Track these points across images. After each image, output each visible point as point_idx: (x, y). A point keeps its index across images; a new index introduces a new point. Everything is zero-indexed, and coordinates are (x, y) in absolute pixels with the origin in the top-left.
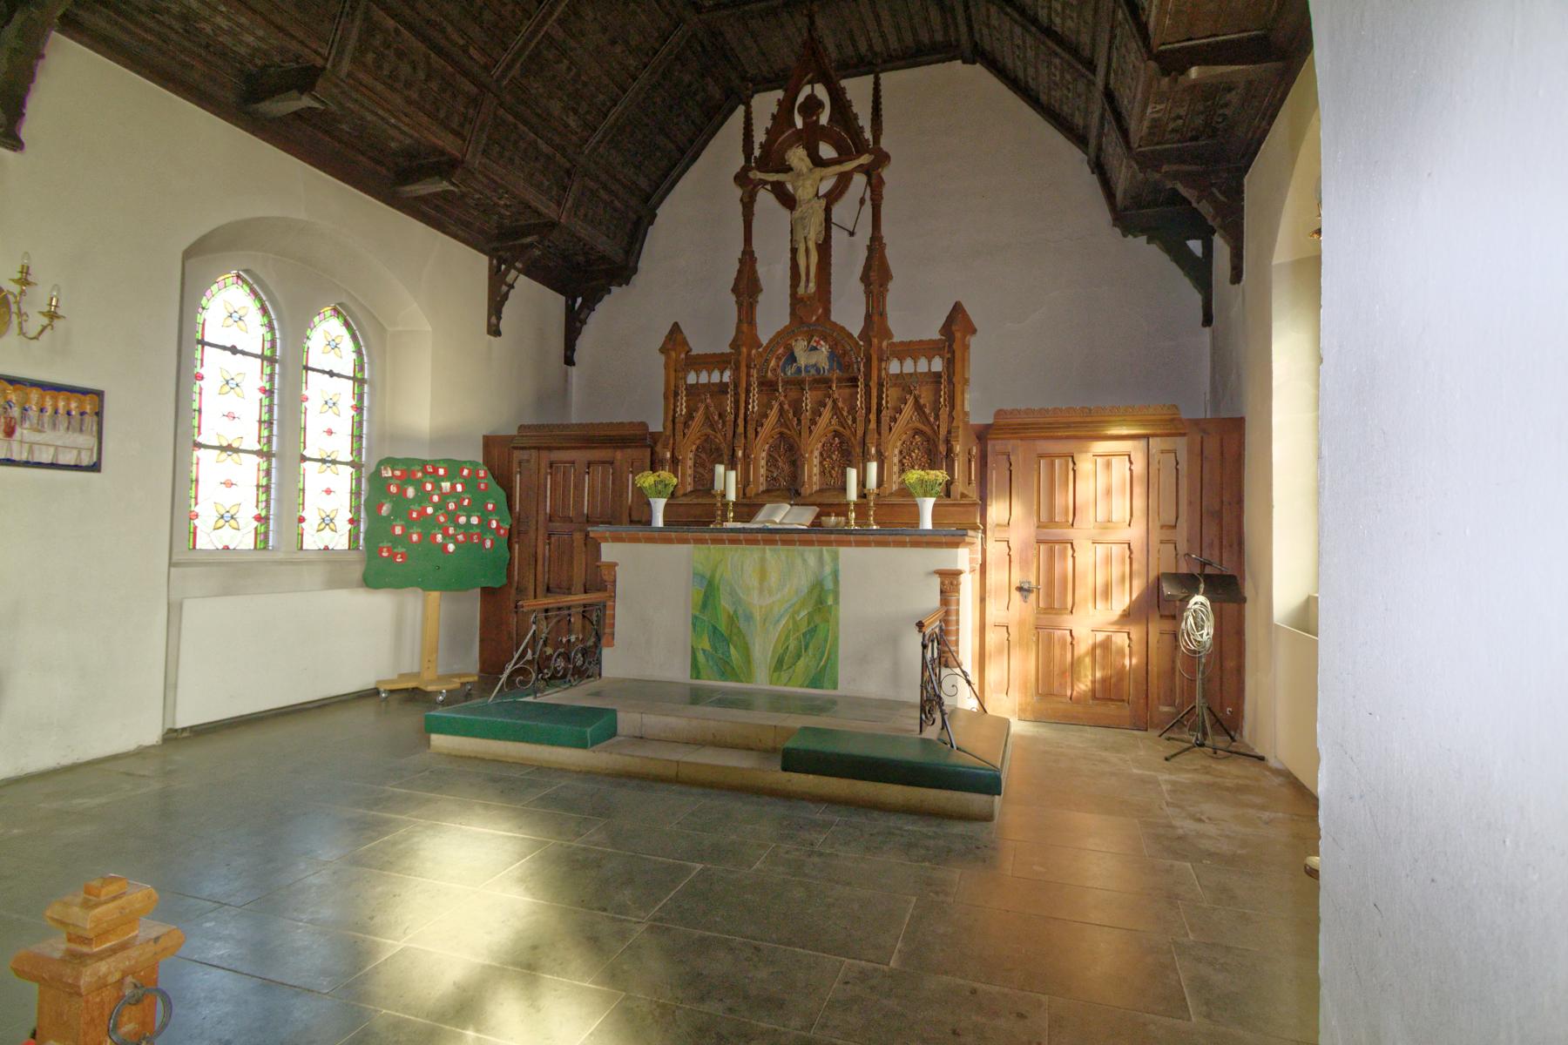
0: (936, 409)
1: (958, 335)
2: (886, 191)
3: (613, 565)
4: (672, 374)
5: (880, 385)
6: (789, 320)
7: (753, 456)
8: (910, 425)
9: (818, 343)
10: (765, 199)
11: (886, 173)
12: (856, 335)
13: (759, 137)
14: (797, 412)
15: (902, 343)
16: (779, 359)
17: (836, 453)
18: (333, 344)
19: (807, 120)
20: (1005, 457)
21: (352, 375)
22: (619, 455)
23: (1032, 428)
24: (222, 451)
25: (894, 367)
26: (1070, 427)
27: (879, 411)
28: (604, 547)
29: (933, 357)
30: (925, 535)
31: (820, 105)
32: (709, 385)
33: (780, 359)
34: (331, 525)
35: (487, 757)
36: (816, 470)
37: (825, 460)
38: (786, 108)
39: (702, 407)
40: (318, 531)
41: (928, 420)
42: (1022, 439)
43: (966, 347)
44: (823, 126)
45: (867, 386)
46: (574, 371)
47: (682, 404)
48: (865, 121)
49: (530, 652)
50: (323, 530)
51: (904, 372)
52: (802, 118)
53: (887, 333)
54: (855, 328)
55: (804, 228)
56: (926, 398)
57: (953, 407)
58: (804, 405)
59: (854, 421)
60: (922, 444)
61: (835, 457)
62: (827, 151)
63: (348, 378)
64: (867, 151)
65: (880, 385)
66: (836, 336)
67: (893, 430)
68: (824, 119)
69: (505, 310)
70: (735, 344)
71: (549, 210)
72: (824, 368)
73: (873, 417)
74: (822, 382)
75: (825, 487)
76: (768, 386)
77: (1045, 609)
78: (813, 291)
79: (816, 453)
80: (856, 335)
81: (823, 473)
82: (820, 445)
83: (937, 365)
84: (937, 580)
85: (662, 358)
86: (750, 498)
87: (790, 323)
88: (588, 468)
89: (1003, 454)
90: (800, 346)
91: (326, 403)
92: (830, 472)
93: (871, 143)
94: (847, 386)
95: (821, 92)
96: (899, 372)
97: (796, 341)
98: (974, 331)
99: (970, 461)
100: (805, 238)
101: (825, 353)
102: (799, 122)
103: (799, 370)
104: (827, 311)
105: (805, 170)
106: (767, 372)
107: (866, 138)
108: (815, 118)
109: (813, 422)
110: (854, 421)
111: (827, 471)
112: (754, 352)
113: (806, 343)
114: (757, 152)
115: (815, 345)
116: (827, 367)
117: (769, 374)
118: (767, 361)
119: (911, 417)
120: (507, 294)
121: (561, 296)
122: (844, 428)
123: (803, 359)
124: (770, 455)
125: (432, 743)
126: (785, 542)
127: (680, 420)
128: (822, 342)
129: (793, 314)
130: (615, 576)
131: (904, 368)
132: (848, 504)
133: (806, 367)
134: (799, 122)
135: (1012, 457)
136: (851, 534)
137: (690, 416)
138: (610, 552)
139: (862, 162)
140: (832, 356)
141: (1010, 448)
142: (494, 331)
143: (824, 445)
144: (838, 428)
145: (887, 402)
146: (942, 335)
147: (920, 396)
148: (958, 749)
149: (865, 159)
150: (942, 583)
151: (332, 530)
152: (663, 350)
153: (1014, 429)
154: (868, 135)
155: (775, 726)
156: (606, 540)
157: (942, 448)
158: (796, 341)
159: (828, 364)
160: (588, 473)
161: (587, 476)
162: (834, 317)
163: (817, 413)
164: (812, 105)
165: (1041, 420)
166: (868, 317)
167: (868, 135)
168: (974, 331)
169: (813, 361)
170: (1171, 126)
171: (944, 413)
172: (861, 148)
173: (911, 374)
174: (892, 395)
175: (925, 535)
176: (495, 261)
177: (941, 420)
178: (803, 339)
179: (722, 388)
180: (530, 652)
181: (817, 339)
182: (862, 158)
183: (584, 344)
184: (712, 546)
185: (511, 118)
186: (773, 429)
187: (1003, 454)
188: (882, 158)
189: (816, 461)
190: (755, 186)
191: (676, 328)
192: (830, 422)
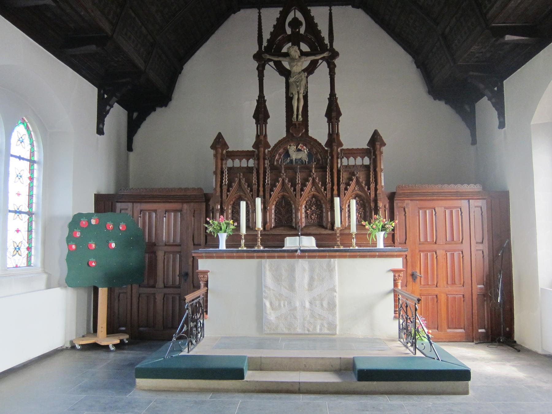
0: (368, 184)
1: (378, 146)
2: (336, 70)
3: (205, 273)
4: (219, 161)
5: (339, 171)
6: (286, 135)
7: (269, 208)
8: (354, 192)
9: (302, 147)
10: (270, 70)
11: (337, 61)
12: (323, 144)
13: (266, 36)
14: (294, 185)
15: (348, 149)
16: (280, 155)
17: (314, 206)
18: (21, 139)
19: (293, 30)
20: (402, 209)
21: (29, 158)
22: (185, 206)
23: (420, 195)
24: (21, 211)
25: (345, 161)
26: (433, 195)
27: (339, 185)
28: (201, 262)
29: (364, 157)
30: (387, 252)
31: (301, 24)
32: (240, 168)
33: (281, 155)
34: (19, 251)
35: (166, 389)
36: (303, 216)
37: (308, 210)
38: (281, 21)
39: (237, 180)
40: (13, 256)
41: (364, 190)
42: (411, 200)
43: (381, 153)
44: (301, 34)
45: (332, 171)
46: (131, 154)
47: (225, 178)
48: (325, 34)
49: (185, 326)
50: (15, 255)
51: (350, 164)
52: (290, 29)
53: (341, 144)
54: (323, 139)
55: (297, 87)
56: (362, 179)
57: (376, 184)
58: (297, 180)
59: (325, 189)
60: (360, 202)
61: (313, 209)
62: (305, 48)
63: (12, 156)
64: (327, 50)
65: (339, 171)
66: (312, 143)
67: (346, 194)
68: (302, 30)
69: (106, 119)
70: (256, 145)
71: (140, 63)
72: (305, 161)
73: (335, 188)
74: (306, 167)
75: (308, 224)
76: (276, 169)
77: (424, 285)
78: (301, 120)
79: (303, 206)
80: (323, 144)
81: (307, 217)
82: (305, 202)
83: (367, 161)
84: (392, 274)
85: (212, 152)
86: (268, 231)
87: (286, 136)
88: (165, 214)
89: (402, 207)
90: (292, 149)
91: (17, 176)
92: (311, 217)
93: (329, 46)
94: (319, 171)
95: (300, 16)
96: (347, 164)
97: (290, 146)
98: (385, 145)
99: (385, 211)
100: (298, 92)
101: (306, 153)
102: (289, 31)
103: (291, 161)
104: (307, 131)
105: (297, 57)
106: (274, 162)
107: (326, 43)
108: (298, 30)
109: (302, 190)
110: (325, 189)
111: (309, 216)
112: (266, 151)
113: (295, 147)
114: (265, 44)
115: (300, 148)
116: (307, 160)
117: (275, 163)
118: (275, 156)
119: (355, 189)
120: (109, 110)
121: (126, 111)
122: (319, 193)
123: (294, 156)
124: (277, 208)
125: (137, 384)
126: (310, 257)
127: (325, 197)
128: (305, 147)
129: (288, 131)
130: (208, 278)
131: (349, 162)
132: (351, 234)
133: (296, 159)
134: (289, 31)
135: (406, 209)
136: (347, 252)
137: (230, 185)
138: (203, 265)
139: (325, 55)
140: (310, 155)
141: (405, 205)
142: (100, 131)
143: (307, 202)
144: (315, 193)
145: (268, 181)
146: (368, 146)
147: (359, 177)
148: (442, 361)
149: (326, 54)
150: (394, 276)
151: (19, 255)
152: (213, 147)
153: (407, 195)
154: (327, 41)
155: (340, 358)
156: (202, 257)
157: (372, 205)
158: (290, 146)
159: (307, 159)
160: (165, 217)
161: (165, 218)
162: (311, 134)
163: (304, 185)
164: (295, 23)
165: (419, 191)
166: (330, 135)
167: (327, 41)
168: (385, 145)
169: (299, 157)
170: (477, 55)
171: (372, 186)
172: (324, 48)
173: (354, 166)
174: (344, 176)
175: (387, 252)
176: (102, 91)
177: (371, 190)
178: (293, 145)
179: (249, 170)
180: (185, 326)
181: (302, 145)
182: (325, 53)
183: (138, 138)
184: (268, 260)
185: (133, 15)
186: (279, 193)
187: (402, 207)
188: (335, 54)
189: (303, 211)
190: (265, 62)
191: (220, 136)
192: (311, 190)
